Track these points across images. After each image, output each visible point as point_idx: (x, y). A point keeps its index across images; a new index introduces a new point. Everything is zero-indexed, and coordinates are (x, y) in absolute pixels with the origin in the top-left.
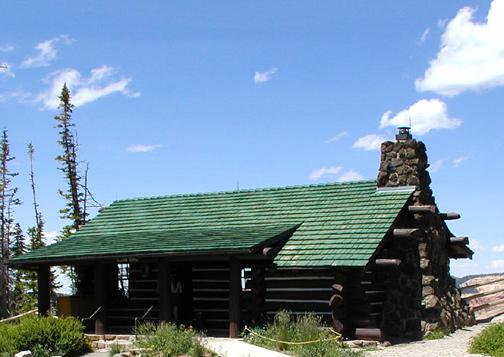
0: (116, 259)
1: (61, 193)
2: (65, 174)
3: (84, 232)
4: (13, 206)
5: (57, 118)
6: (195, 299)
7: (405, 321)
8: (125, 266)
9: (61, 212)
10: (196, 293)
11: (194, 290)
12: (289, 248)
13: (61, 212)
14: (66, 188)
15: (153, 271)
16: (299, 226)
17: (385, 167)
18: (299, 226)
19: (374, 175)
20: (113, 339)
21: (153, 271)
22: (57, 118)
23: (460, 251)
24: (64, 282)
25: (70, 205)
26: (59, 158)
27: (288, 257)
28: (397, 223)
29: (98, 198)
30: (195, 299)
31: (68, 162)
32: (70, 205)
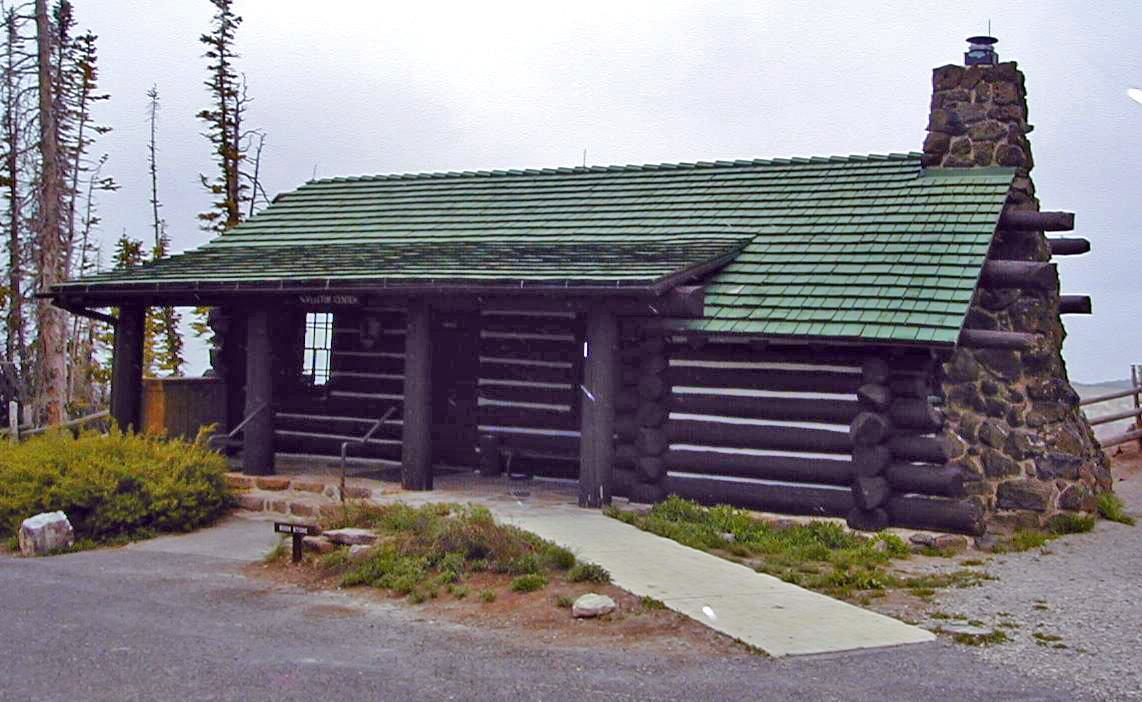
0: (296, 296)
1: (204, 179)
2: (214, 147)
3: (240, 241)
4: (100, 195)
5: (206, 39)
6: (482, 402)
7: (994, 485)
8: (321, 317)
9: (203, 217)
10: (484, 387)
11: (482, 381)
12: (733, 288)
13: (203, 217)
14: (216, 175)
15: (386, 332)
16: (750, 242)
17: (943, 121)
18: (750, 242)
19: (912, 139)
20: (284, 487)
21: (386, 332)
22: (206, 39)
23: (1084, 308)
24: (191, 346)
25: (219, 206)
26: (205, 114)
27: (726, 313)
28: (997, 250)
29: (275, 174)
30: (482, 402)
31: (223, 124)
32: (219, 206)
